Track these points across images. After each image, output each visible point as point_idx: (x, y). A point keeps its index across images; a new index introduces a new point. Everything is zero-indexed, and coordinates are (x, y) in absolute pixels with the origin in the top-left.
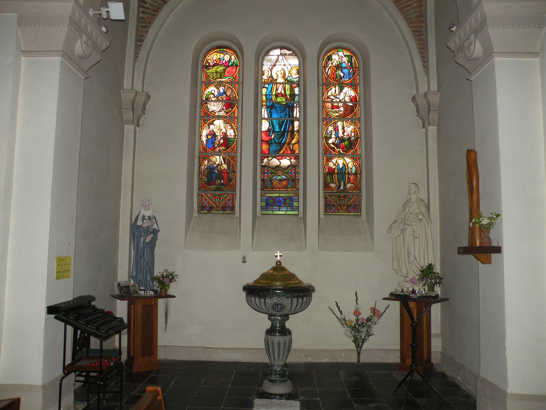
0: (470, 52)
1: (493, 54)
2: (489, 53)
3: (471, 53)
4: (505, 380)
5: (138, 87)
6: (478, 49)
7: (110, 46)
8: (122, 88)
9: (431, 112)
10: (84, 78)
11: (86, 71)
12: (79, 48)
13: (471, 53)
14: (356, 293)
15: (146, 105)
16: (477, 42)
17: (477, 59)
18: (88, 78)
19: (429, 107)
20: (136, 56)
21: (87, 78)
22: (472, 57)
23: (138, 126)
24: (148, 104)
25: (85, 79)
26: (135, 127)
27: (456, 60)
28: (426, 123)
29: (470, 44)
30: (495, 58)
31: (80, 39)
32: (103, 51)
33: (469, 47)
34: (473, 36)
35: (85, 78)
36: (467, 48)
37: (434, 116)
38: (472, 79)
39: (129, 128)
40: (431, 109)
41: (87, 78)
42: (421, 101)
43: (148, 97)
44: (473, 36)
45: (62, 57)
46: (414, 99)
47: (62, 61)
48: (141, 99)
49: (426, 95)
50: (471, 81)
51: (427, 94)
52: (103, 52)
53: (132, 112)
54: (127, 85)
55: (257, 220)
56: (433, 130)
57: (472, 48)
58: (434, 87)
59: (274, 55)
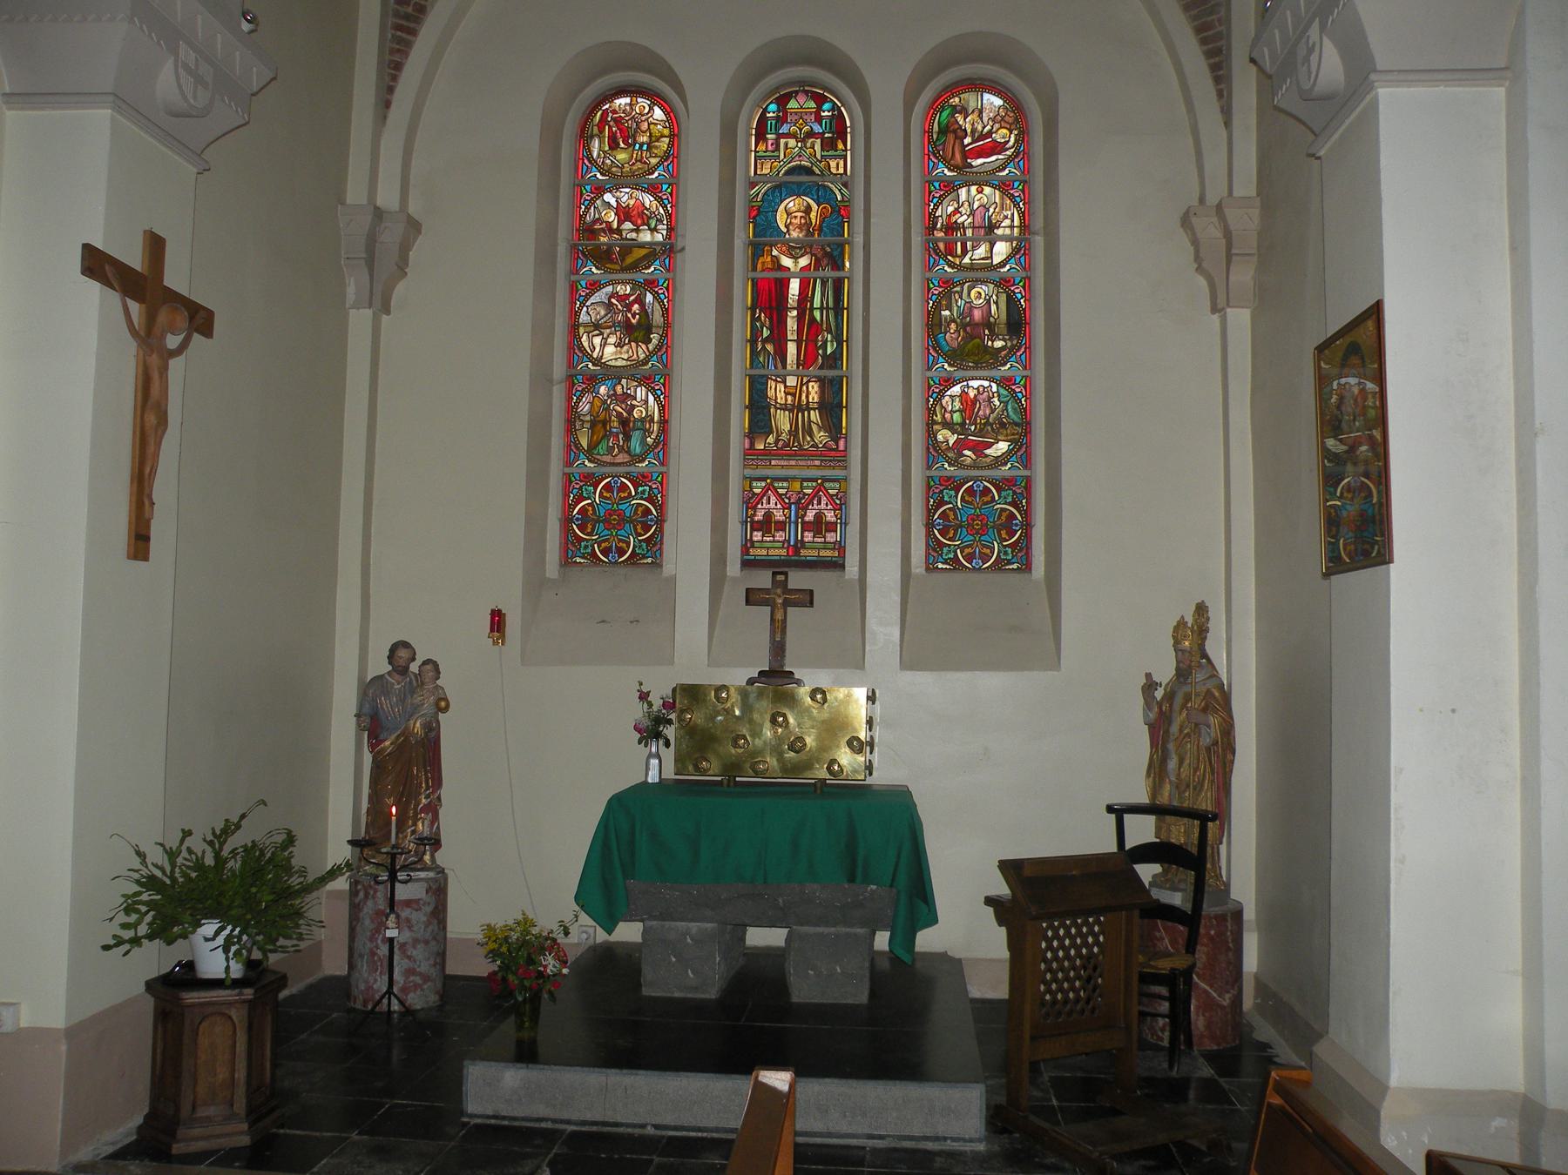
0: (1310, 73)
1: (1373, 77)
2: (1361, 72)
3: (1313, 76)
4: (1388, 1076)
5: (388, 198)
6: (1330, 67)
7: (274, 79)
8: (343, 203)
9: (1234, 258)
10: (195, 170)
11: (199, 153)
12: (167, 83)
13: (1313, 76)
14: (211, 950)
15: (411, 250)
16: (1327, 43)
17: (1327, 98)
18: (208, 170)
19: (1229, 246)
20: (385, 103)
21: (204, 170)
22: (1316, 89)
23: (388, 312)
24: (413, 245)
25: (199, 173)
26: (374, 313)
27: (1278, 101)
28: (1221, 302)
29: (1311, 50)
30: (1380, 90)
31: (171, 61)
32: (253, 95)
33: (1307, 60)
34: (1316, 24)
35: (201, 171)
36: (1303, 65)
37: (1243, 275)
38: (1322, 153)
39: (359, 321)
40: (1234, 251)
41: (204, 170)
42: (1209, 230)
43: (414, 226)
44: (1316, 24)
45: (113, 109)
46: (1186, 221)
47: (113, 119)
48: (391, 236)
49: (1219, 208)
50: (1319, 158)
51: (1223, 205)
52: (254, 97)
53: (366, 270)
54: (355, 194)
55: (726, 588)
56: (1240, 318)
57: (1314, 58)
58: (1246, 185)
59: (1228, 124)
